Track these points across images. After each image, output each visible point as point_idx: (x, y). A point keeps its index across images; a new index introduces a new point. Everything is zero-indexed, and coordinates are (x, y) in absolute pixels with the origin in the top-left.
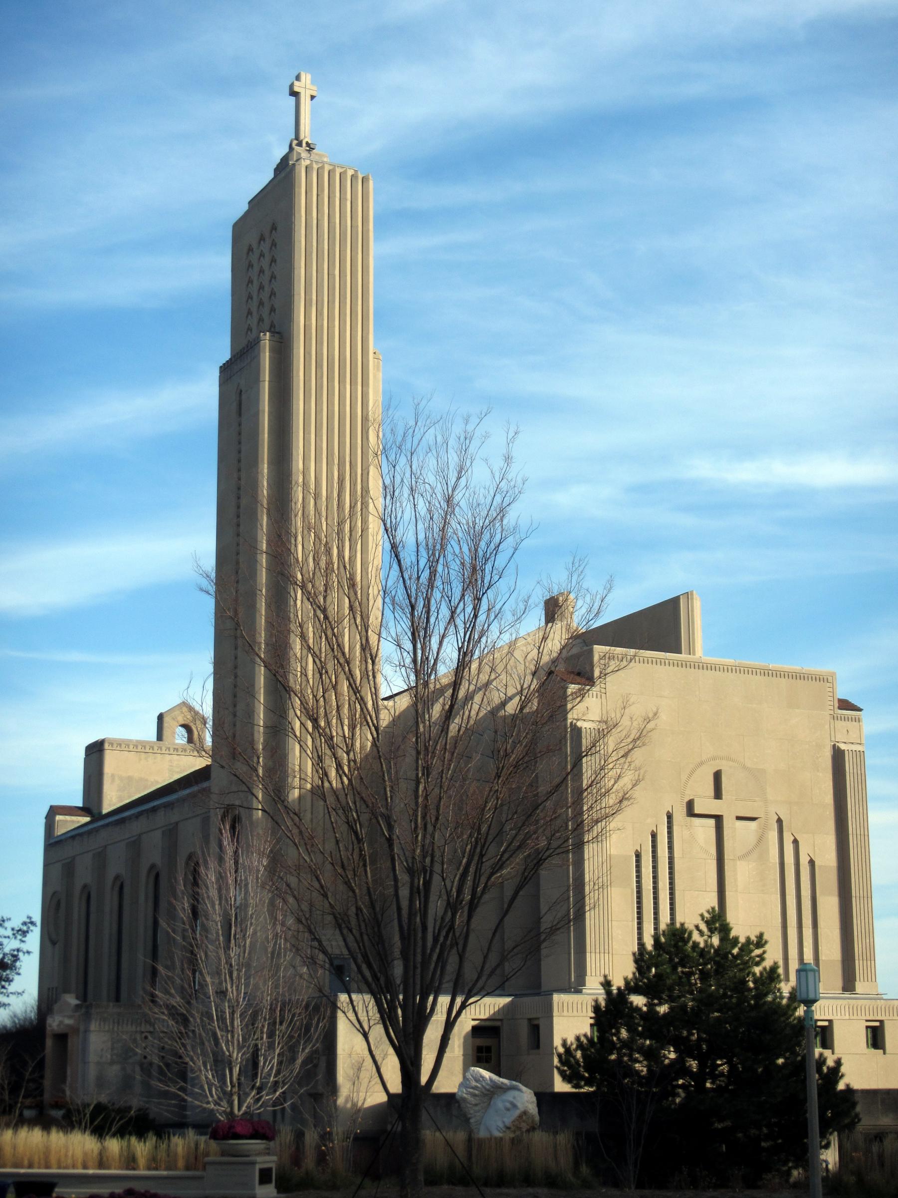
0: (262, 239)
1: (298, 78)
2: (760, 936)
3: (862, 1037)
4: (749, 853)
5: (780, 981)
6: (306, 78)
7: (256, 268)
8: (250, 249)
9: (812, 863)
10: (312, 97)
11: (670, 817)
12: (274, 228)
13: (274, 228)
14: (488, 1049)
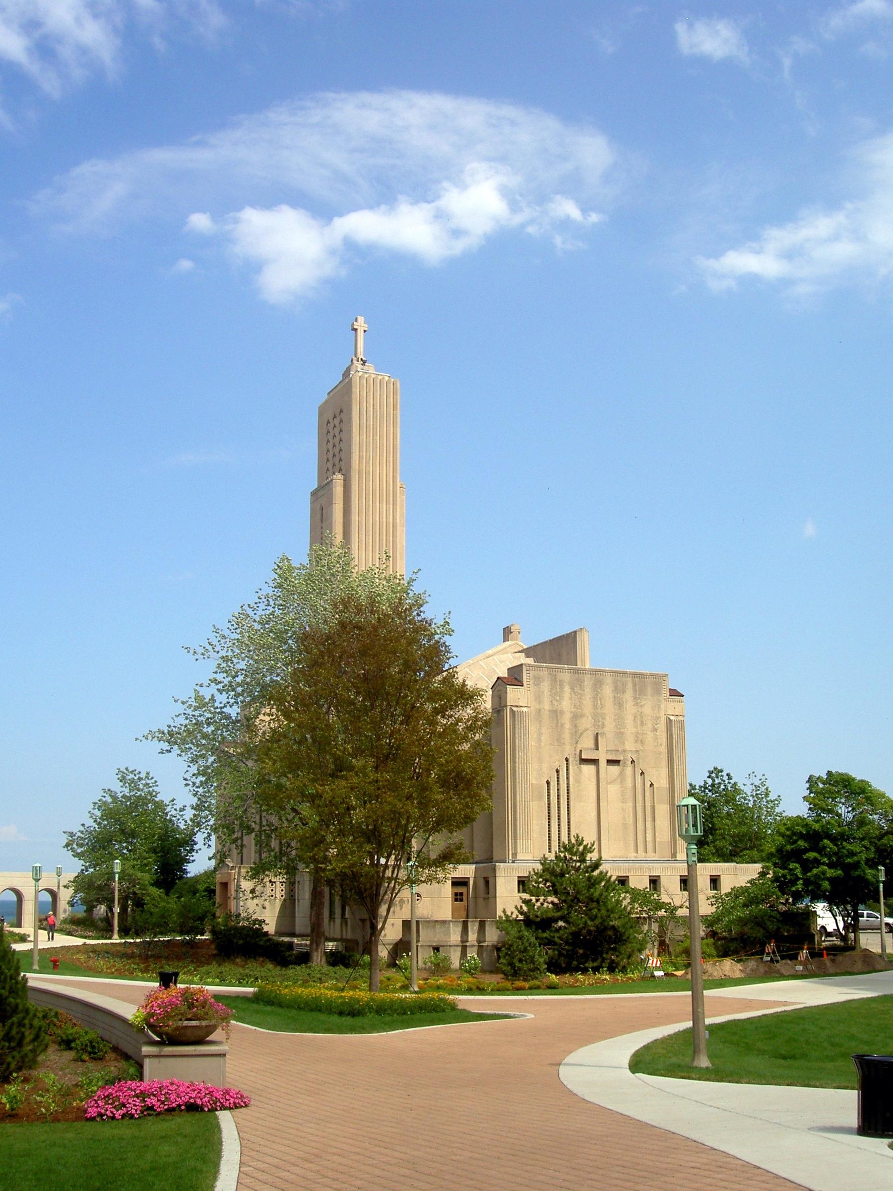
0: (335, 417)
1: (356, 321)
2: (691, 785)
3: (663, 881)
4: (615, 780)
5: (710, 922)
6: (361, 319)
7: (331, 434)
8: (328, 422)
9: (652, 785)
10: (365, 331)
11: (567, 760)
12: (341, 411)
13: (341, 411)
14: (461, 894)
